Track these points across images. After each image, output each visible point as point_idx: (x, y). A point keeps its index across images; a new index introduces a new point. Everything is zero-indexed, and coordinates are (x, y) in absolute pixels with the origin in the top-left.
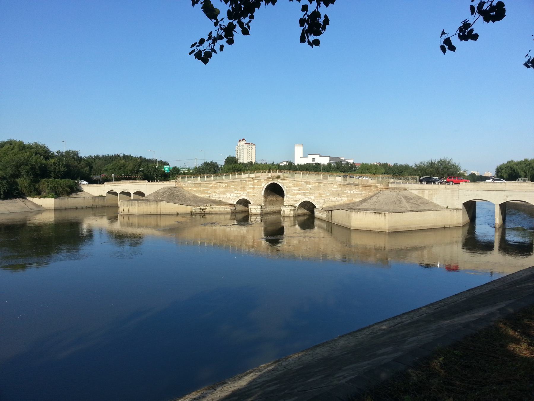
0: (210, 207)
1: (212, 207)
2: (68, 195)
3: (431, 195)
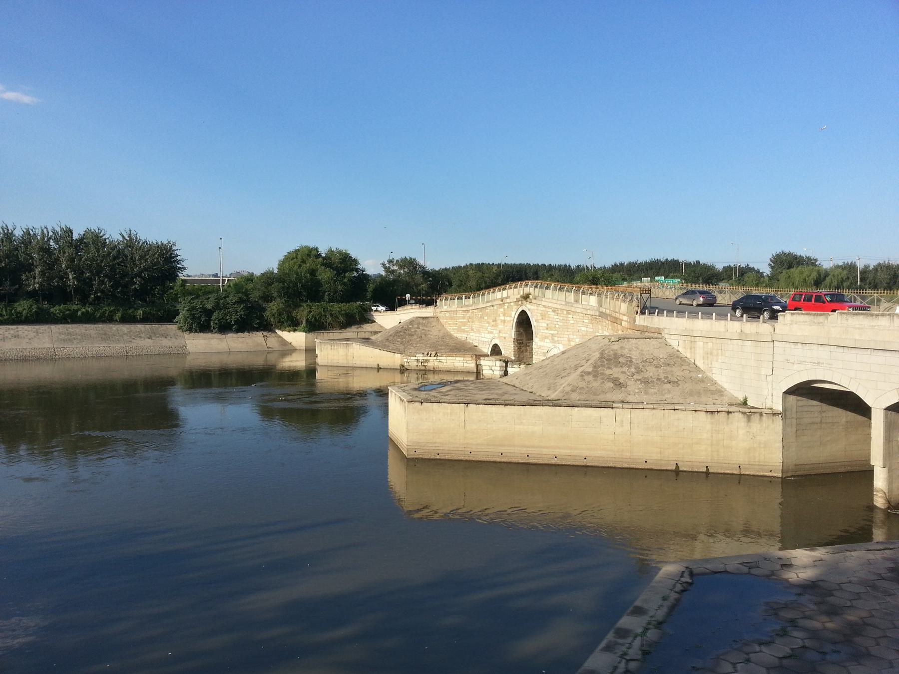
0: (435, 358)
1: (438, 358)
2: (341, 329)
3: (709, 356)
